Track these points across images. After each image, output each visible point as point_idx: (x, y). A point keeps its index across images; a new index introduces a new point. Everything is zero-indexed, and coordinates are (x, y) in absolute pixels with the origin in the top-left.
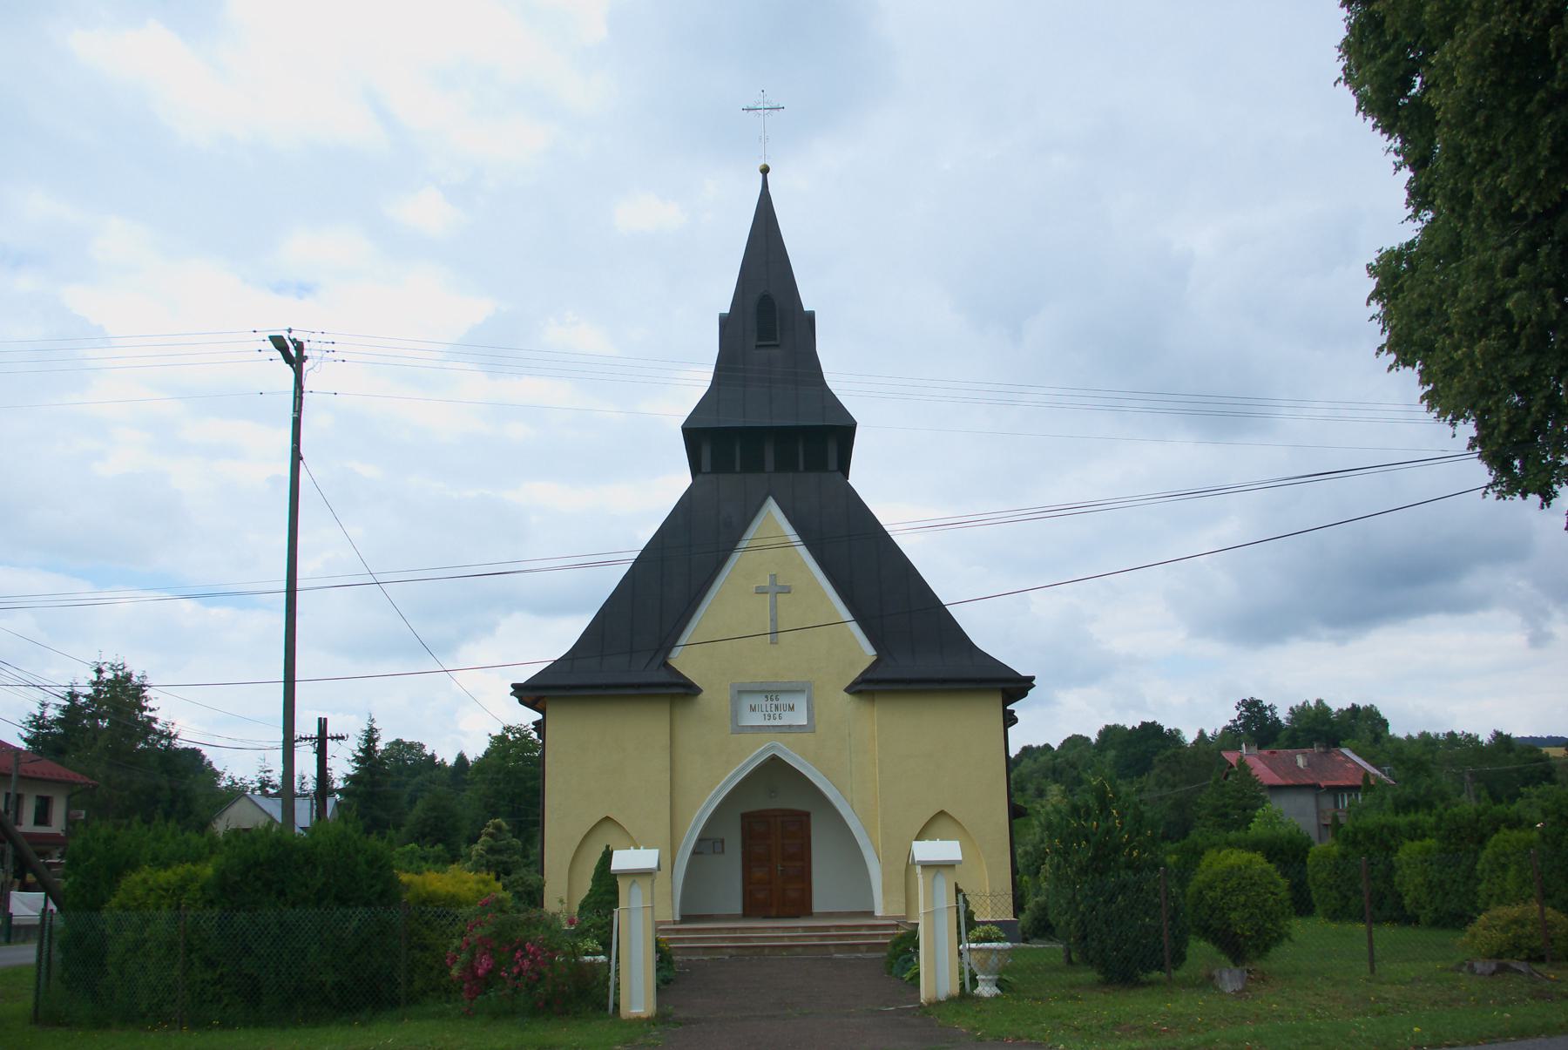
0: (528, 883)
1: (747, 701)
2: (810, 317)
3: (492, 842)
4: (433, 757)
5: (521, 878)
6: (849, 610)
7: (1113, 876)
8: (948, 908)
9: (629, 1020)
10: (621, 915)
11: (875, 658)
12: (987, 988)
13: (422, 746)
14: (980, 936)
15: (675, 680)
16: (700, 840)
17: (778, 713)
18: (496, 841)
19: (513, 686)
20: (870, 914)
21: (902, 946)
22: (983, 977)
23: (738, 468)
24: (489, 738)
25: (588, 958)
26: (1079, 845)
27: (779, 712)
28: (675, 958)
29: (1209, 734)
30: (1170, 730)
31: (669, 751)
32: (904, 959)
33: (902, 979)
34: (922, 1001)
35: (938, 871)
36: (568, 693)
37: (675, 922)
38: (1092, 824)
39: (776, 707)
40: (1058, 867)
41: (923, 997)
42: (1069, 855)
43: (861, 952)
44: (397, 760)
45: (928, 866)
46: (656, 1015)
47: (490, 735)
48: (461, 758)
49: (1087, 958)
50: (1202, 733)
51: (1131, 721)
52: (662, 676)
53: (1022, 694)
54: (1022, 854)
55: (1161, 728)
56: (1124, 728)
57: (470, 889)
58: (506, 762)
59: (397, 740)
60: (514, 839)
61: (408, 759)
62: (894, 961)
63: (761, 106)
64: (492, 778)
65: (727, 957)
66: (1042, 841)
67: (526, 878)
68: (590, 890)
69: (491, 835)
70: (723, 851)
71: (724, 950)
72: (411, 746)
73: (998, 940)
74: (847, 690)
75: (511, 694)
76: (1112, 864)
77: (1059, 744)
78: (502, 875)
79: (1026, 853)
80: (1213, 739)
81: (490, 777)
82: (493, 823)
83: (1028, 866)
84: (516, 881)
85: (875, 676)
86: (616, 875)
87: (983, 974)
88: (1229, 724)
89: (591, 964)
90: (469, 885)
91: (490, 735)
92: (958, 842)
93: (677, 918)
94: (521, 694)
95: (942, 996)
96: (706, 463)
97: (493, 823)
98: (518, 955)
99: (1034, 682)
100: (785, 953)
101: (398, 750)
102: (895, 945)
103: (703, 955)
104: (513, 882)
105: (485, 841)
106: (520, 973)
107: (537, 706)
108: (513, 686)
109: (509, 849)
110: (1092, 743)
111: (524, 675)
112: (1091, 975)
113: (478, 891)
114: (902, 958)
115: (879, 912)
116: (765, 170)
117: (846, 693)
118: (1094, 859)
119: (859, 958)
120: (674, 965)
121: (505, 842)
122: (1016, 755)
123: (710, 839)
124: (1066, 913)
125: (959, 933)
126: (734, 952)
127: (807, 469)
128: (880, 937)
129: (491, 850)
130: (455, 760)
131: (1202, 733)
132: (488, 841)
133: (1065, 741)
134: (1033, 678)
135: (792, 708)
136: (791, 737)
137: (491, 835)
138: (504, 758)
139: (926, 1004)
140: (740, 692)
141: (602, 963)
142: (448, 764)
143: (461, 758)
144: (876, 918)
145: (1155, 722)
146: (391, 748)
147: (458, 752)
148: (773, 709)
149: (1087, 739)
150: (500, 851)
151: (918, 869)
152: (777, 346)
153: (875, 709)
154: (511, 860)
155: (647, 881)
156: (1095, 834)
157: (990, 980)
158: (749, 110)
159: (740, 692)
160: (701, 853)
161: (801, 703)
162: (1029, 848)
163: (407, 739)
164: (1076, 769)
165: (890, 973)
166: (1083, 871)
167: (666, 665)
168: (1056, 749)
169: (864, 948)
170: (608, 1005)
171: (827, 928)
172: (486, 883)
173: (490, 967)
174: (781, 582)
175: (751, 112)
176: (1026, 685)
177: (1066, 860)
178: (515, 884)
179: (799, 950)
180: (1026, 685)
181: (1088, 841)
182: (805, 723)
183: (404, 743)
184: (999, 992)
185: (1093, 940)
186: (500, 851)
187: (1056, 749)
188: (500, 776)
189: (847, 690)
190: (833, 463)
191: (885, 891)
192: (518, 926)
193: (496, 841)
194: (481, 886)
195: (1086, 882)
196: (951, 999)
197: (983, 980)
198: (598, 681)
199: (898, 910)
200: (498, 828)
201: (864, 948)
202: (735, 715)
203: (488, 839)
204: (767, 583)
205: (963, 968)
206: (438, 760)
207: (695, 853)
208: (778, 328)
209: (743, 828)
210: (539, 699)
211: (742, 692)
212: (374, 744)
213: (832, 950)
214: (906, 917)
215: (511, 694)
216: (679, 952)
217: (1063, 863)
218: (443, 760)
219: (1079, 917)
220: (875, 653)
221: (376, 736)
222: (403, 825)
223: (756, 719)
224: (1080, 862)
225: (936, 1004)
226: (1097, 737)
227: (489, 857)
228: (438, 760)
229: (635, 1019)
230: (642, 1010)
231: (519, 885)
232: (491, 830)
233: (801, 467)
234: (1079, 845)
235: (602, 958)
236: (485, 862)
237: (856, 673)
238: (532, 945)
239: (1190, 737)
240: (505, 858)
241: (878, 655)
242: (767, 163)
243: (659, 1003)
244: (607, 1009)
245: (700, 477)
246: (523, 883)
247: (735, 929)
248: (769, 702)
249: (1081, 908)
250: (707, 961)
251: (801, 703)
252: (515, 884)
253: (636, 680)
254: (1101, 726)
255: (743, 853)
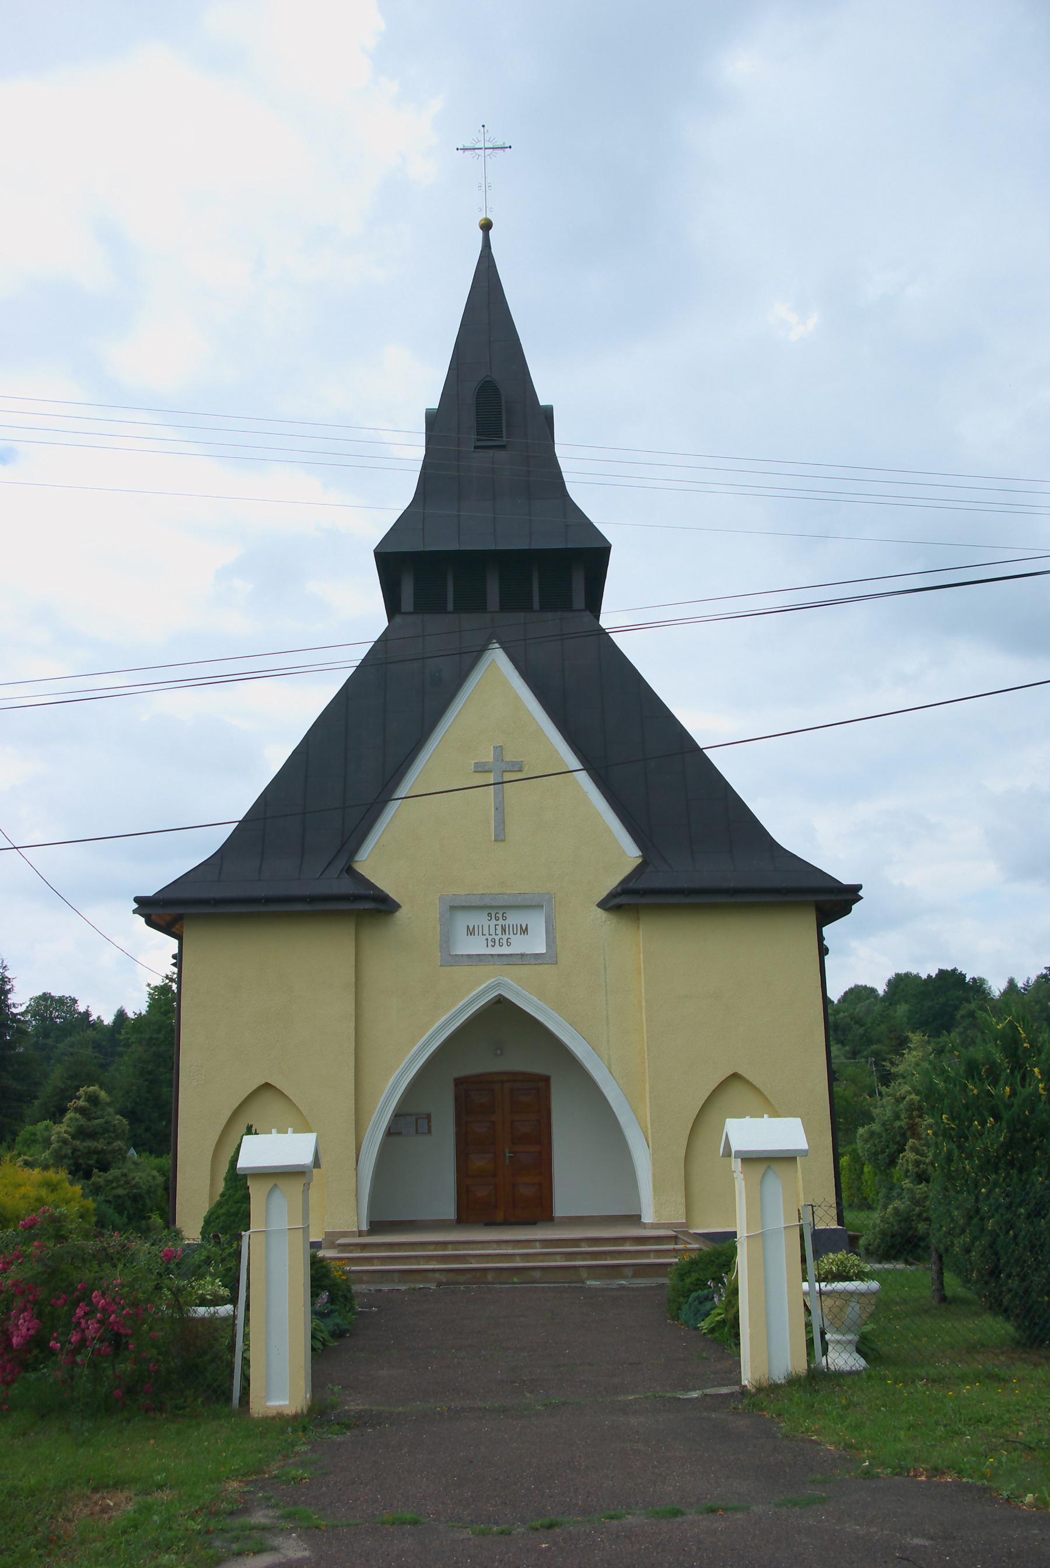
0: (133, 1183)
1: (463, 921)
2: (548, 414)
3: (83, 1121)
4: (87, 1014)
5: (125, 1175)
6: (602, 793)
7: (1040, 1173)
8: (785, 1227)
9: (265, 1419)
10: (252, 1242)
11: (640, 860)
12: (845, 1355)
13: (75, 1001)
14: (831, 1271)
15: (362, 891)
16: (397, 1115)
17: (505, 937)
18: (89, 1120)
19: (137, 900)
20: (635, 1219)
21: (694, 1276)
22: (838, 1337)
23: (450, 606)
24: (148, 989)
25: (201, 1311)
26: (983, 1123)
27: (507, 936)
28: (356, 1288)
29: (1020, 985)
30: (974, 979)
31: (353, 990)
32: (698, 1297)
33: (697, 1329)
34: (745, 1382)
35: (769, 1167)
36: (212, 910)
37: (360, 1234)
38: (1004, 1089)
39: (504, 930)
40: (949, 1159)
41: (747, 1378)
42: (967, 1139)
43: (625, 1277)
44: (43, 1019)
45: (750, 1159)
46: (311, 1409)
47: (149, 985)
48: (121, 1015)
49: (1000, 1305)
50: (1012, 983)
51: (927, 970)
52: (345, 886)
53: (844, 909)
54: (866, 1136)
55: (963, 976)
56: (917, 977)
57: (24, 1197)
58: (168, 1018)
59: (44, 994)
60: (118, 1117)
61: (57, 1017)
62: (682, 1299)
63: (488, 152)
64: (151, 1039)
65: (433, 1286)
66: (897, 1117)
67: (132, 1175)
68: (222, 1195)
69: (82, 1111)
70: (429, 1132)
71: (430, 1275)
72: (61, 1001)
73: (861, 1276)
74: (603, 905)
75: (135, 912)
76: (1038, 1153)
77: (839, 997)
78: (95, 1170)
79: (872, 1134)
80: (1025, 989)
81: (147, 1036)
82: (86, 1093)
83: (876, 1154)
84: (116, 1179)
85: (642, 884)
86: (245, 1177)
87: (838, 1330)
88: (1044, 972)
89: (212, 1319)
90: (23, 1190)
91: (149, 985)
92: (727, 1120)
93: (365, 1227)
94: (147, 911)
95: (779, 1377)
96: (407, 601)
97: (86, 1093)
98: (79, 1312)
99: (861, 893)
100: (515, 1280)
101: (46, 1006)
102: (683, 1272)
103: (400, 1282)
104: (112, 1182)
105: (71, 1119)
106: (83, 1343)
107: (174, 930)
108: (137, 900)
109: (107, 1131)
110: (879, 995)
111: (150, 892)
112: (1000, 1328)
113: (37, 1200)
114: (694, 1294)
115: (648, 1218)
116: (486, 226)
117: (599, 909)
118: (1008, 1146)
119: (623, 1288)
120: (356, 1302)
121: (103, 1120)
122: (936, 975)
123: (411, 1115)
124: (963, 1231)
125: (804, 1260)
126: (443, 1278)
127: (543, 608)
128: (652, 1254)
129: (81, 1133)
130: (114, 1017)
131: (1012, 983)
132: (77, 1120)
133: (846, 993)
134: (859, 887)
135: (524, 931)
136: (524, 971)
137: (82, 1111)
138: (166, 1013)
139: (754, 1390)
140: (453, 908)
141: (225, 1319)
142: (106, 1023)
143: (121, 1015)
144: (645, 1226)
145: (955, 970)
146: (38, 1004)
147: (118, 1007)
148: (499, 931)
149: (873, 991)
150: (93, 1135)
151: (737, 1165)
152: (502, 447)
153: (641, 926)
154: (110, 1148)
155: (295, 1187)
156: (1009, 1107)
157: (850, 1342)
158: (464, 149)
159: (453, 908)
160: (399, 1134)
161: (537, 923)
162: (876, 1127)
163: (56, 993)
164: (862, 1025)
165: (676, 1317)
166: (990, 1164)
167: (350, 870)
168: (836, 1002)
169: (629, 1272)
170: (231, 1391)
171: (576, 1242)
172: (52, 1187)
173: (32, 1332)
174: (508, 758)
175: (466, 152)
176: (851, 897)
177: (960, 1147)
178: (114, 1184)
179: (537, 1274)
180: (851, 897)
181: (997, 1118)
182: (544, 951)
183: (52, 998)
184: (862, 1362)
185: (1009, 1276)
186: (93, 1135)
187: (836, 1002)
188: (161, 1036)
189: (603, 905)
190: (579, 599)
191: (658, 1188)
192: (84, 1261)
193: (89, 1120)
194: (43, 1192)
195: (996, 1184)
196: (793, 1381)
197: (838, 1342)
198: (295, 890)
199: (676, 1215)
200: (93, 1100)
201: (629, 1272)
202: (446, 939)
203: (78, 1116)
204: (490, 759)
205: (645, 1228)
206: (94, 1017)
207: (390, 1133)
208: (504, 424)
209: (457, 1098)
210: (179, 918)
211: (456, 907)
212: (6, 997)
213: (584, 1274)
214: (686, 1225)
215: (135, 912)
216: (365, 1278)
217: (956, 1152)
218: (99, 1017)
219: (985, 1241)
220: (640, 853)
221: (8, 987)
222: (36, 1098)
223: (475, 946)
224: (986, 1149)
225: (769, 1390)
226: (885, 987)
227: (77, 1143)
228: (94, 1017)
229: (273, 1418)
230: (287, 1403)
231: (119, 1186)
232: (82, 1103)
233: (536, 605)
234: (983, 1123)
235: (225, 1310)
236: (69, 1152)
237: (611, 882)
238: (103, 1294)
239: (997, 987)
240: (100, 1145)
241: (643, 856)
242: (488, 217)
243: (318, 1380)
244: (229, 1399)
245: (399, 619)
246: (127, 1183)
247: (444, 1244)
248: (494, 922)
249: (990, 1224)
250: (405, 1292)
251: (537, 923)
252: (114, 1184)
253: (308, 892)
254: (890, 974)
255: (458, 1134)
